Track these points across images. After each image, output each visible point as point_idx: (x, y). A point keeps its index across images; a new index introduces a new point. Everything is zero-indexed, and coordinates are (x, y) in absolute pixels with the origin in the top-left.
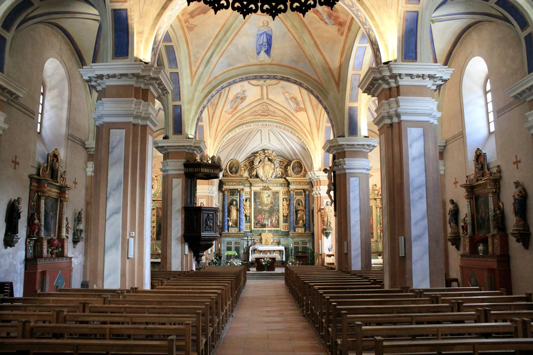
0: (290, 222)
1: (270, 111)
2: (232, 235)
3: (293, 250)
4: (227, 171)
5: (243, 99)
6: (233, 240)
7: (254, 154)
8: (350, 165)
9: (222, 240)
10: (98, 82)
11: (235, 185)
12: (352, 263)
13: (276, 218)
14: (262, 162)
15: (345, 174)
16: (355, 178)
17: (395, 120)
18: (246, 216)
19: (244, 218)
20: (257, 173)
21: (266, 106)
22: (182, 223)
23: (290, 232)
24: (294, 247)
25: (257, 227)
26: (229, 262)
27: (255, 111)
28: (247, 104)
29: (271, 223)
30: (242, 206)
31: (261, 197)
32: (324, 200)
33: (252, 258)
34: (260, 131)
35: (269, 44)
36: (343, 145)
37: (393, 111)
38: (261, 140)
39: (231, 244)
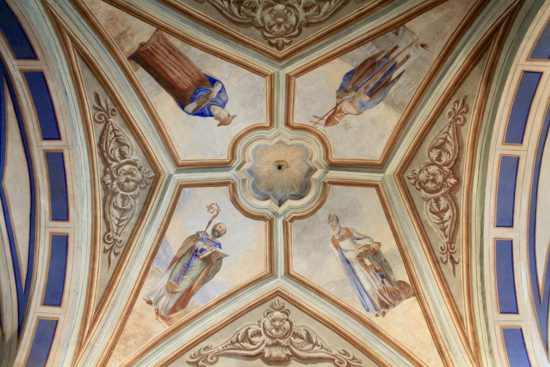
1: (296, 335)
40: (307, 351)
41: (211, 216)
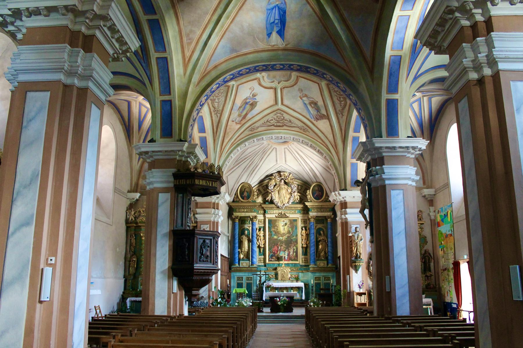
0: (310, 254)
1: (285, 120)
2: (244, 269)
3: (314, 286)
4: (237, 197)
5: (253, 105)
6: (244, 275)
7: (269, 177)
8: (390, 174)
9: (232, 275)
10: (15, 24)
11: (247, 212)
12: (397, 305)
13: (294, 249)
14: (277, 186)
15: (384, 187)
16: (398, 192)
17: (487, 72)
18: (259, 247)
19: (256, 250)
20: (271, 199)
21: (280, 114)
22: (169, 251)
23: (310, 266)
24: (315, 283)
25: (273, 260)
26: (236, 302)
27: (268, 120)
28: (258, 112)
29: (288, 255)
30: (255, 235)
31: (276, 226)
32: (352, 226)
33: (266, 295)
34: (274, 150)
35: (283, 22)
36: (381, 148)
37: (483, 57)
38: (277, 161)
39: (243, 280)
40: (290, 124)
41: (251, 91)
